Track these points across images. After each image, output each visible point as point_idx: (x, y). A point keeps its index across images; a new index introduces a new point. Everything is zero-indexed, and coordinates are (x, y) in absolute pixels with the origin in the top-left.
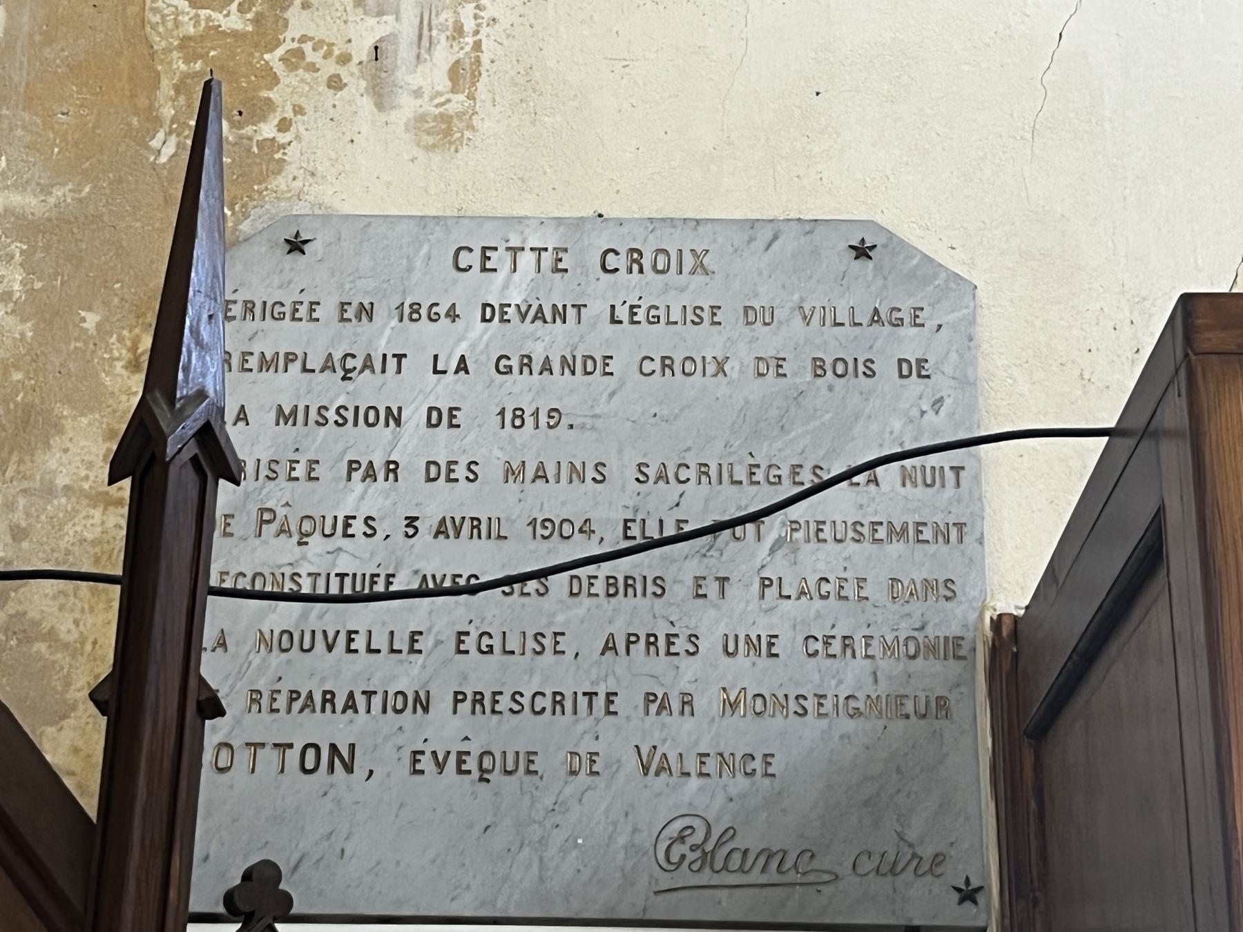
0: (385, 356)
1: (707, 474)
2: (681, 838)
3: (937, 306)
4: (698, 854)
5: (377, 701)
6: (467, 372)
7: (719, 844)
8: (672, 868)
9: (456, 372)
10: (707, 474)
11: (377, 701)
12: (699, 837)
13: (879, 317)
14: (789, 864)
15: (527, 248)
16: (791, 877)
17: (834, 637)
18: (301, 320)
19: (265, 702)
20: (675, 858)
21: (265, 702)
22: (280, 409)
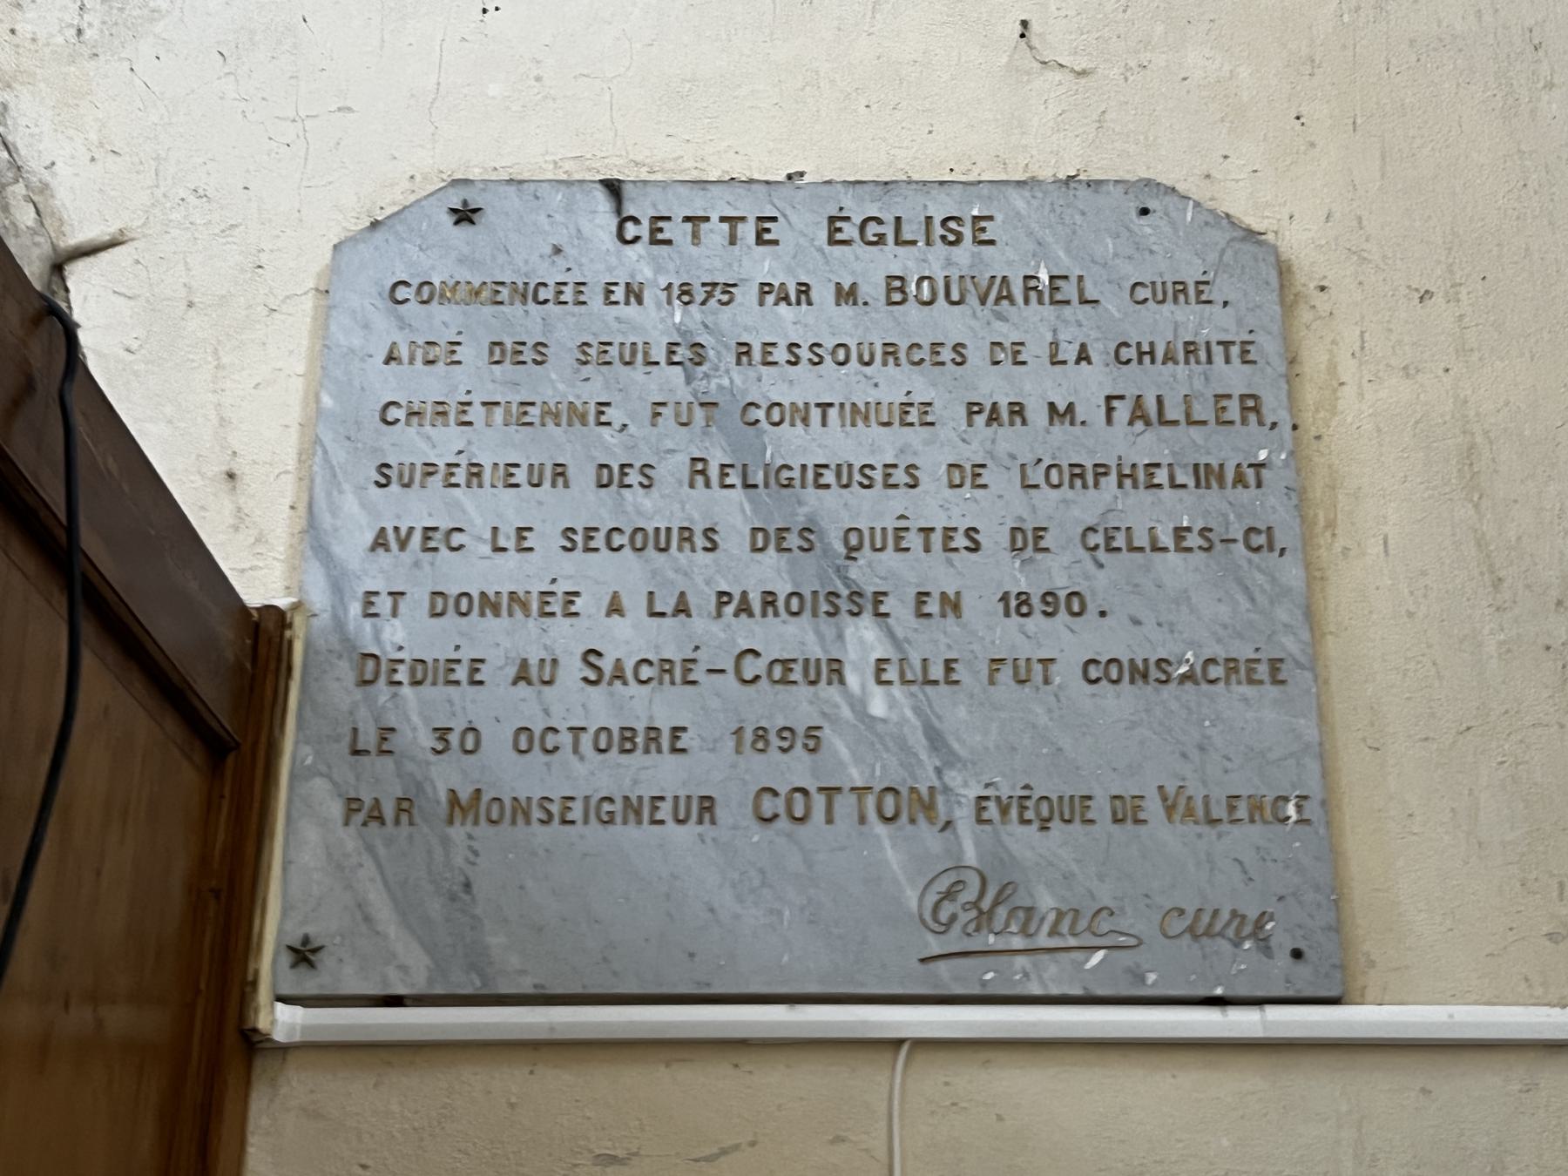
0: (1208, 344)
1: (702, 472)
2: (949, 895)
3: (1191, 276)
4: (974, 913)
5: (586, 740)
6: (1090, 363)
7: (996, 903)
8: (942, 929)
9: (1078, 362)
10: (702, 472)
11: (586, 740)
12: (970, 895)
13: (1009, 291)
14: (1083, 924)
15: (715, 218)
16: (1043, 940)
17: (458, 661)
18: (616, 303)
19: (665, 742)
20: (943, 917)
21: (665, 742)
22: (1052, 406)
